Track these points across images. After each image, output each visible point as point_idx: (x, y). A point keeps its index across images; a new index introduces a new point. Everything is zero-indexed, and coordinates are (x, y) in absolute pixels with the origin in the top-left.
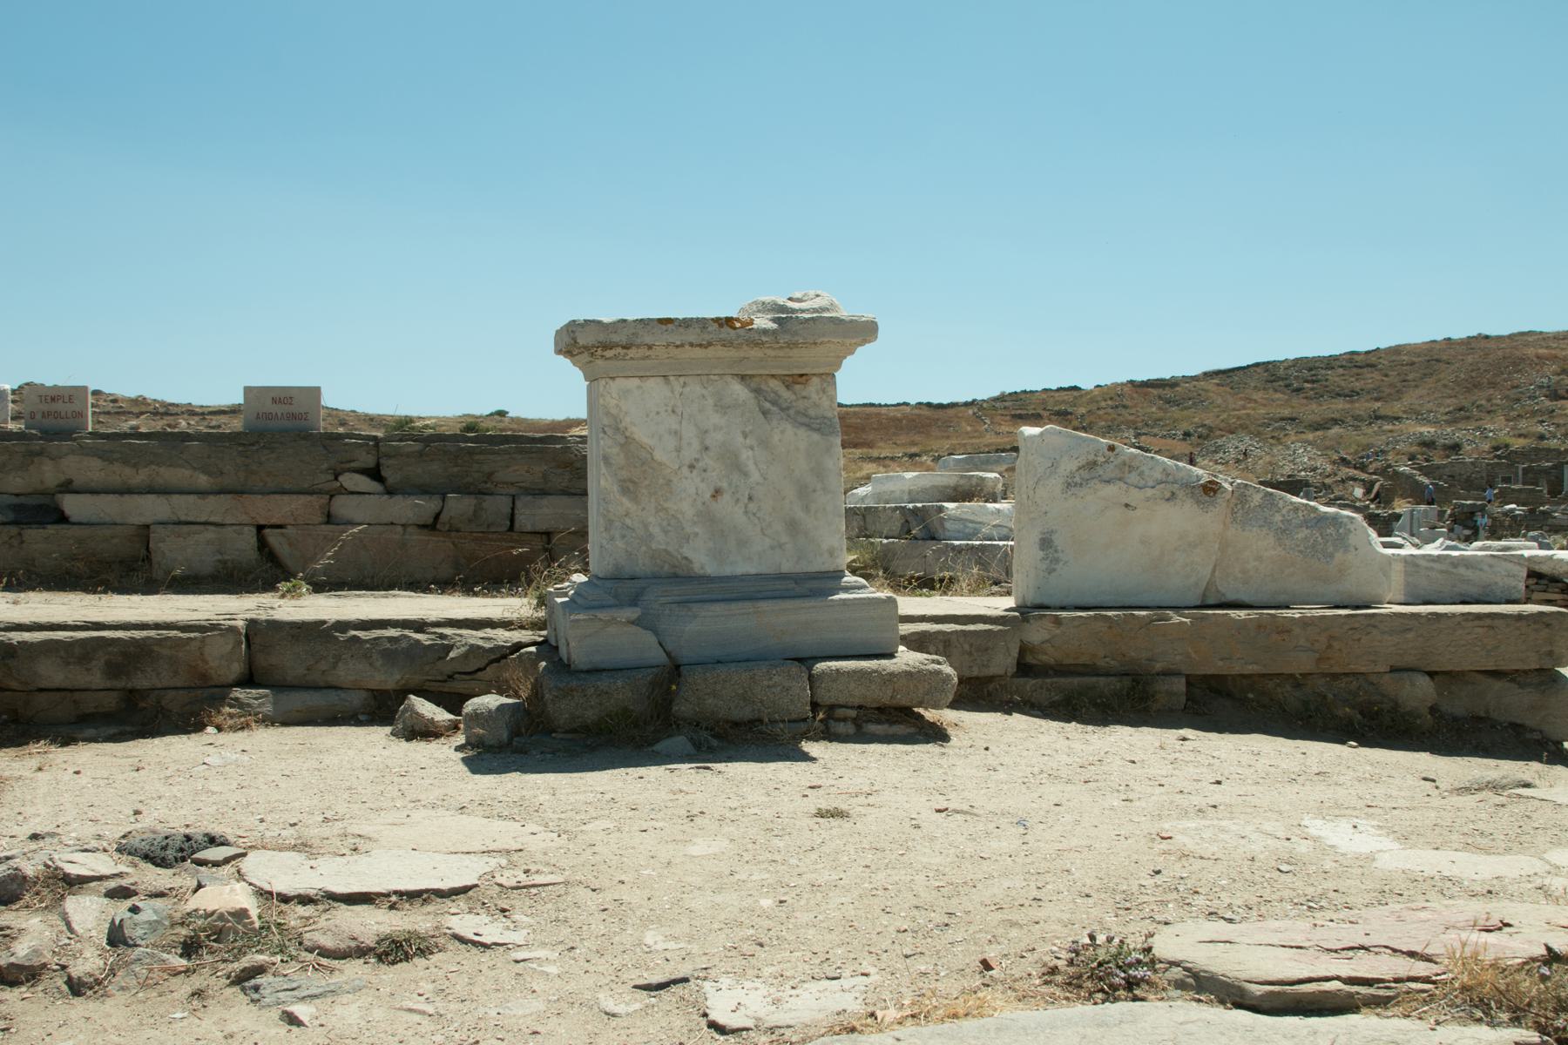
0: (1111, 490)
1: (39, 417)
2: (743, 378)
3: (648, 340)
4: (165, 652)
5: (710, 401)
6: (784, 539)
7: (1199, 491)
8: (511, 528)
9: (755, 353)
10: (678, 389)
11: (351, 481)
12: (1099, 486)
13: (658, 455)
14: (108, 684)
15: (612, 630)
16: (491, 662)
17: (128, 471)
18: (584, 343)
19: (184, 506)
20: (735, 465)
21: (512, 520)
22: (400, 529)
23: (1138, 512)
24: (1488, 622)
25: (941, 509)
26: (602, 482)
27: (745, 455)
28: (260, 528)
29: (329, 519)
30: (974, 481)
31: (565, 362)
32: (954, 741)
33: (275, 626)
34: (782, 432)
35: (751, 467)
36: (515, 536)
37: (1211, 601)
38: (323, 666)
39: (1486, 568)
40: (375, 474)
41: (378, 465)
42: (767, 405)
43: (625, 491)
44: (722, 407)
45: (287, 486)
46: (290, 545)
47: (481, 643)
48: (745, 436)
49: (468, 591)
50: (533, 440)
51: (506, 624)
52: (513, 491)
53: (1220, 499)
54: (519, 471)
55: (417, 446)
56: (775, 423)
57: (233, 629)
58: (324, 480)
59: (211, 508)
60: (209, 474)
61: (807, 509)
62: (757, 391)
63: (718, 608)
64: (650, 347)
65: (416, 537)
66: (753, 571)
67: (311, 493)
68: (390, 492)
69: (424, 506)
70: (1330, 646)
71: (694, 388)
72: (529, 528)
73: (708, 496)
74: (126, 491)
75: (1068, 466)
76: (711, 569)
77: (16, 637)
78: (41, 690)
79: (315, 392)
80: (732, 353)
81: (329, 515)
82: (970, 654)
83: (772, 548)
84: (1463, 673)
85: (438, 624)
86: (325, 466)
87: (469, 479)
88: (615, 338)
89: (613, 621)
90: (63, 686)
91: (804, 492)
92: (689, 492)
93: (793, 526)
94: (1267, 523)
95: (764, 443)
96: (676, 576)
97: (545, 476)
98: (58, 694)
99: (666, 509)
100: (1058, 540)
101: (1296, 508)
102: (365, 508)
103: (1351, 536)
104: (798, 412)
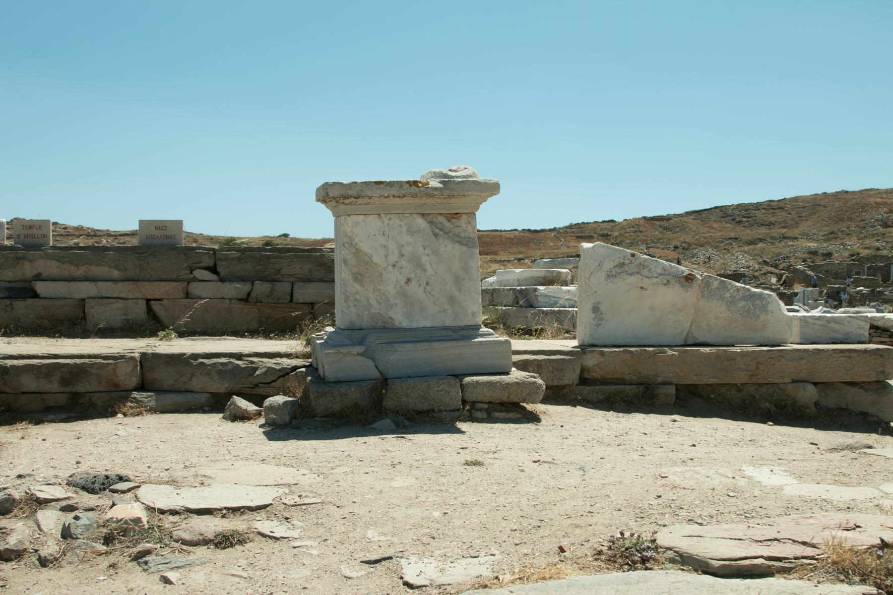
0: (633, 279)
1: (22, 237)
2: (423, 215)
3: (369, 193)
4: (94, 371)
5: (405, 229)
6: (447, 307)
7: (683, 280)
8: (291, 301)
9: (430, 201)
10: (386, 221)
11: (200, 274)
12: (626, 277)
13: (375, 259)
14: (62, 390)
15: (349, 358)
16: (280, 377)
17: (73, 268)
18: (333, 195)
19: (105, 288)
20: (419, 265)
21: (292, 296)
22: (228, 301)
23: (648, 292)
24: (848, 354)
25: (536, 290)
26: (343, 275)
27: (424, 259)
28: (148, 301)
29: (188, 295)
30: (555, 274)
31: (322, 206)
32: (543, 422)
33: (157, 356)
34: (446, 246)
35: (428, 266)
36: (293, 305)
37: (690, 342)
38: (184, 379)
39: (846, 323)
40: (213, 270)
41: (215, 265)
42: (437, 231)
43: (356, 279)
44: (411, 232)
45: (163, 277)
46: (165, 310)
47: (274, 366)
48: (424, 248)
49: (267, 336)
50: (304, 251)
51: (288, 356)
52: (292, 279)
53: (695, 284)
54: (296, 268)
55: (238, 254)
56: (441, 241)
57: (133, 358)
58: (184, 274)
59: (120, 289)
60: (119, 270)
61: (459, 290)
62: (431, 223)
63: (409, 346)
64: (370, 198)
65: (237, 306)
66: (429, 325)
67: (177, 281)
68: (222, 280)
69: (241, 288)
70: (757, 368)
71: (395, 221)
72: (301, 301)
73: (403, 282)
74: (72, 279)
75: (608, 265)
76: (405, 324)
77: (9, 363)
78: (23, 393)
79: (179, 223)
80: (417, 201)
81: (187, 293)
82: (553, 372)
83: (440, 312)
84: (833, 383)
85: (249, 355)
86: (185, 265)
87: (267, 273)
88: (351, 193)
89: (349, 354)
90: (36, 390)
91: (458, 280)
92: (392, 280)
93: (452, 300)
94: (722, 298)
95: (435, 252)
96: (385, 328)
97: (310, 271)
98: (33, 395)
99: (379, 290)
100: (603, 308)
101: (738, 289)
102: (208, 289)
103: (770, 305)
104: (454, 235)
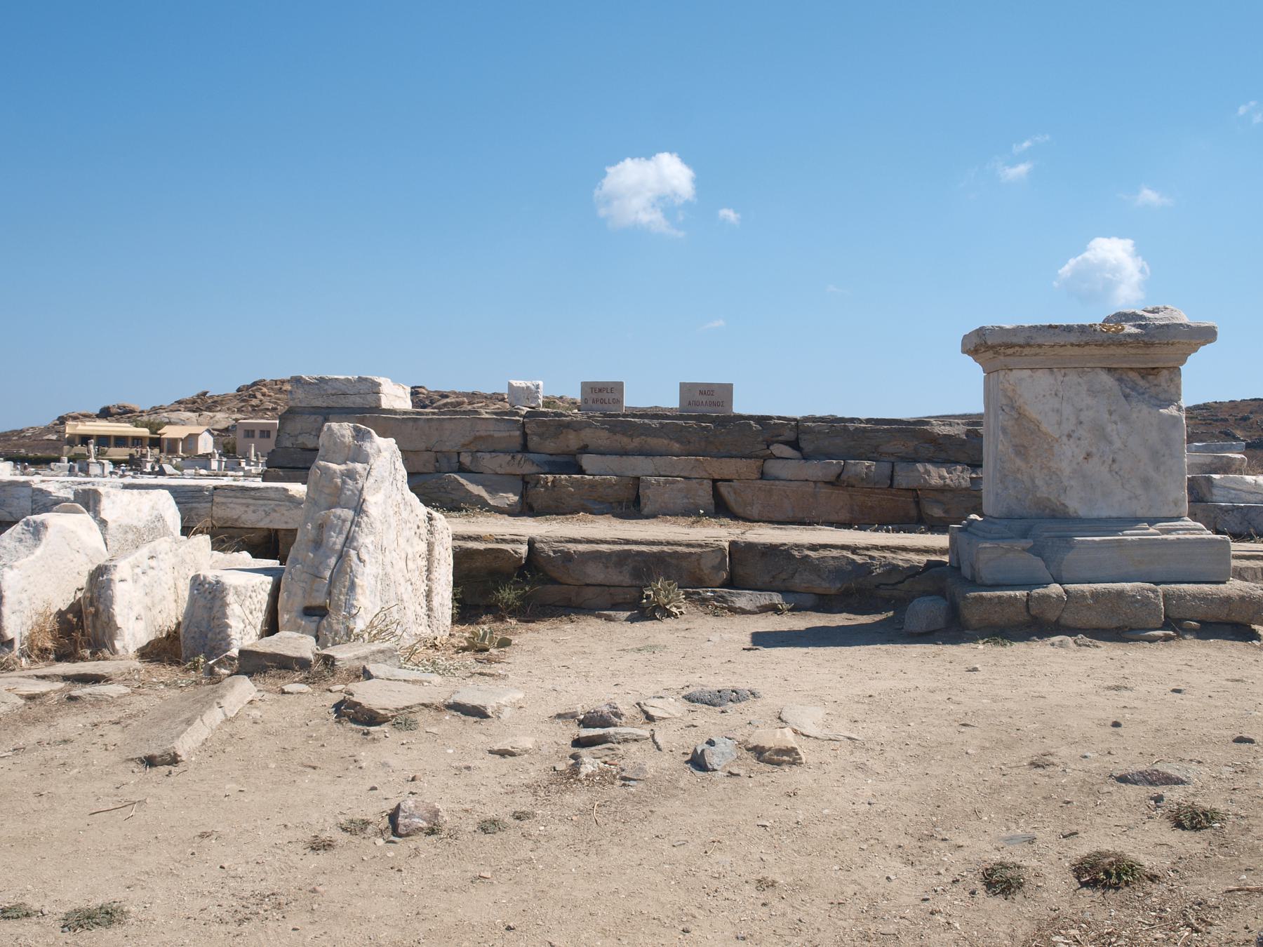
1: (590, 402)
2: (1109, 370)
3: (1040, 341)
4: (674, 562)
8: (891, 486)
9: (1120, 351)
10: (1060, 378)
11: (778, 449)
13: (1044, 427)
15: (1010, 555)
17: (625, 440)
18: (985, 346)
20: (1100, 433)
21: (892, 478)
25: (1210, 480)
26: (1000, 447)
27: (1110, 428)
29: (763, 476)
30: (1225, 461)
31: (969, 359)
33: (750, 546)
34: (1140, 411)
36: (894, 491)
40: (794, 445)
41: (797, 439)
42: (1128, 391)
43: (1018, 453)
44: (1092, 392)
47: (900, 563)
48: (1111, 413)
49: (862, 528)
52: (892, 459)
56: (1134, 404)
57: (722, 550)
61: (1157, 469)
62: (1120, 380)
64: (1040, 346)
65: (825, 490)
66: (1114, 515)
68: (806, 457)
71: (1073, 378)
72: (904, 486)
74: (624, 453)
76: (1083, 512)
78: (588, 585)
80: (1104, 351)
81: (762, 473)
83: (1130, 498)
85: (867, 549)
86: (761, 439)
88: (1015, 340)
92: (1067, 457)
93: (1146, 482)
95: (1125, 419)
99: (1049, 468)
102: (788, 468)
104: (1151, 397)
